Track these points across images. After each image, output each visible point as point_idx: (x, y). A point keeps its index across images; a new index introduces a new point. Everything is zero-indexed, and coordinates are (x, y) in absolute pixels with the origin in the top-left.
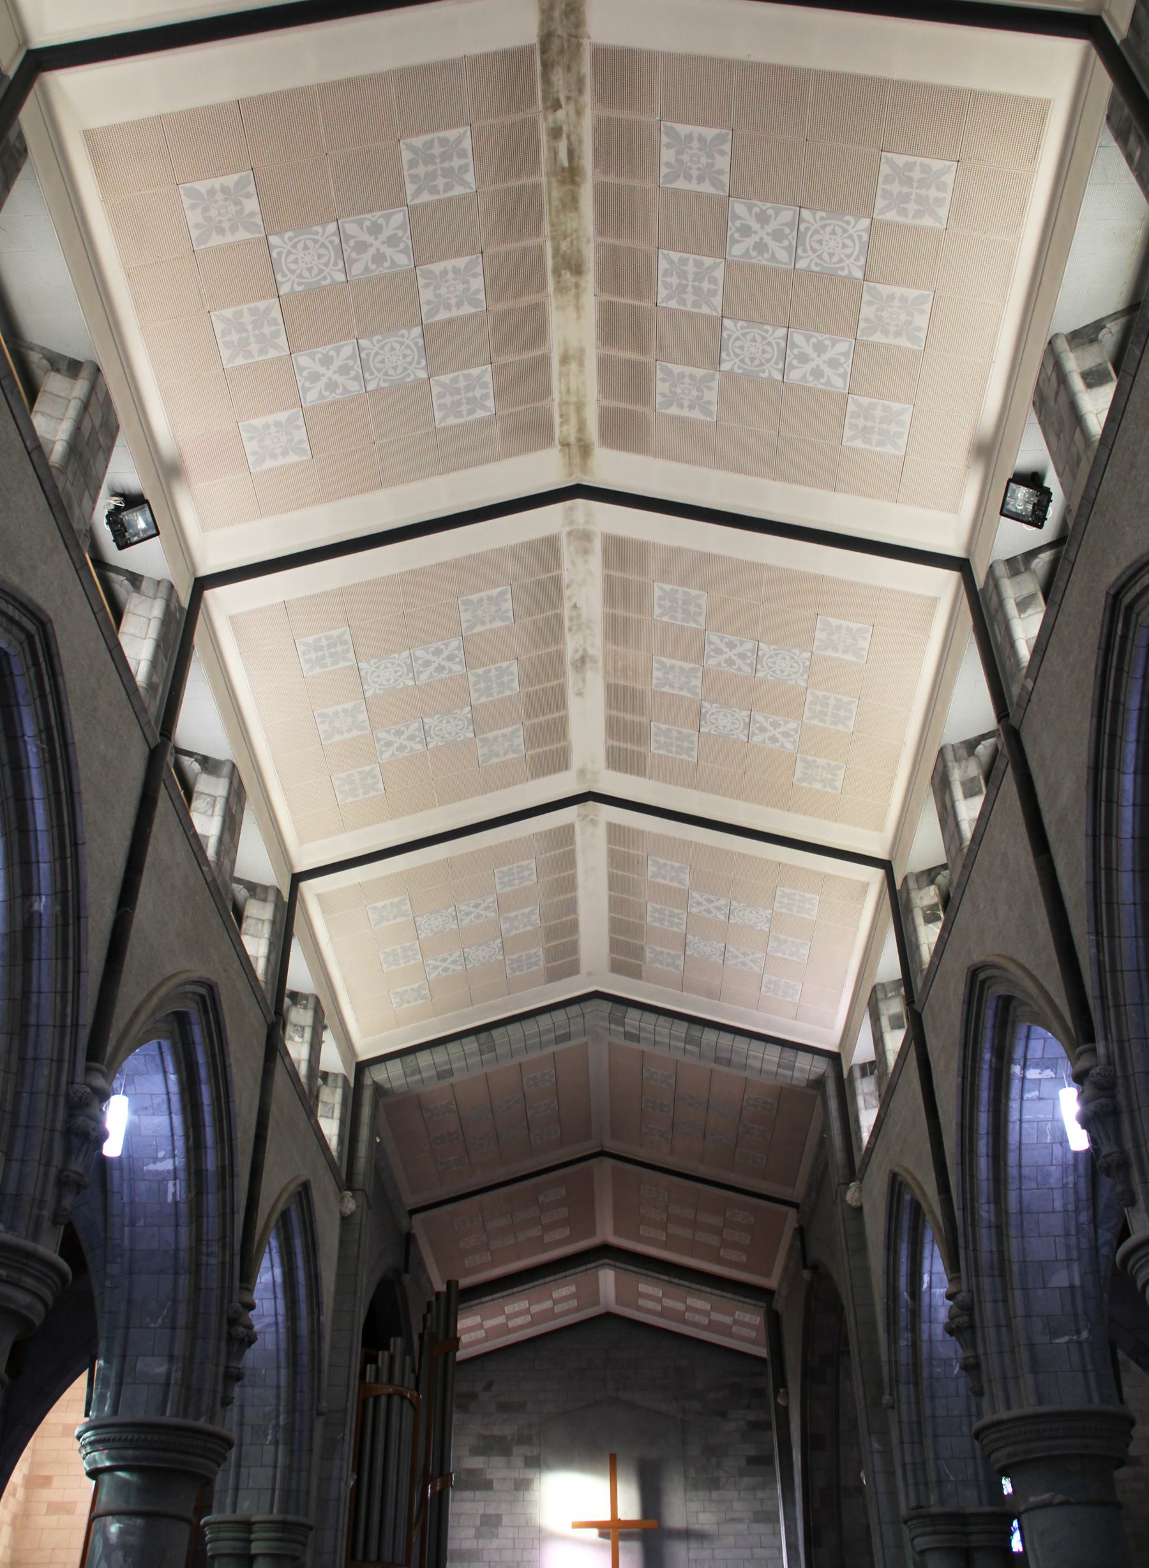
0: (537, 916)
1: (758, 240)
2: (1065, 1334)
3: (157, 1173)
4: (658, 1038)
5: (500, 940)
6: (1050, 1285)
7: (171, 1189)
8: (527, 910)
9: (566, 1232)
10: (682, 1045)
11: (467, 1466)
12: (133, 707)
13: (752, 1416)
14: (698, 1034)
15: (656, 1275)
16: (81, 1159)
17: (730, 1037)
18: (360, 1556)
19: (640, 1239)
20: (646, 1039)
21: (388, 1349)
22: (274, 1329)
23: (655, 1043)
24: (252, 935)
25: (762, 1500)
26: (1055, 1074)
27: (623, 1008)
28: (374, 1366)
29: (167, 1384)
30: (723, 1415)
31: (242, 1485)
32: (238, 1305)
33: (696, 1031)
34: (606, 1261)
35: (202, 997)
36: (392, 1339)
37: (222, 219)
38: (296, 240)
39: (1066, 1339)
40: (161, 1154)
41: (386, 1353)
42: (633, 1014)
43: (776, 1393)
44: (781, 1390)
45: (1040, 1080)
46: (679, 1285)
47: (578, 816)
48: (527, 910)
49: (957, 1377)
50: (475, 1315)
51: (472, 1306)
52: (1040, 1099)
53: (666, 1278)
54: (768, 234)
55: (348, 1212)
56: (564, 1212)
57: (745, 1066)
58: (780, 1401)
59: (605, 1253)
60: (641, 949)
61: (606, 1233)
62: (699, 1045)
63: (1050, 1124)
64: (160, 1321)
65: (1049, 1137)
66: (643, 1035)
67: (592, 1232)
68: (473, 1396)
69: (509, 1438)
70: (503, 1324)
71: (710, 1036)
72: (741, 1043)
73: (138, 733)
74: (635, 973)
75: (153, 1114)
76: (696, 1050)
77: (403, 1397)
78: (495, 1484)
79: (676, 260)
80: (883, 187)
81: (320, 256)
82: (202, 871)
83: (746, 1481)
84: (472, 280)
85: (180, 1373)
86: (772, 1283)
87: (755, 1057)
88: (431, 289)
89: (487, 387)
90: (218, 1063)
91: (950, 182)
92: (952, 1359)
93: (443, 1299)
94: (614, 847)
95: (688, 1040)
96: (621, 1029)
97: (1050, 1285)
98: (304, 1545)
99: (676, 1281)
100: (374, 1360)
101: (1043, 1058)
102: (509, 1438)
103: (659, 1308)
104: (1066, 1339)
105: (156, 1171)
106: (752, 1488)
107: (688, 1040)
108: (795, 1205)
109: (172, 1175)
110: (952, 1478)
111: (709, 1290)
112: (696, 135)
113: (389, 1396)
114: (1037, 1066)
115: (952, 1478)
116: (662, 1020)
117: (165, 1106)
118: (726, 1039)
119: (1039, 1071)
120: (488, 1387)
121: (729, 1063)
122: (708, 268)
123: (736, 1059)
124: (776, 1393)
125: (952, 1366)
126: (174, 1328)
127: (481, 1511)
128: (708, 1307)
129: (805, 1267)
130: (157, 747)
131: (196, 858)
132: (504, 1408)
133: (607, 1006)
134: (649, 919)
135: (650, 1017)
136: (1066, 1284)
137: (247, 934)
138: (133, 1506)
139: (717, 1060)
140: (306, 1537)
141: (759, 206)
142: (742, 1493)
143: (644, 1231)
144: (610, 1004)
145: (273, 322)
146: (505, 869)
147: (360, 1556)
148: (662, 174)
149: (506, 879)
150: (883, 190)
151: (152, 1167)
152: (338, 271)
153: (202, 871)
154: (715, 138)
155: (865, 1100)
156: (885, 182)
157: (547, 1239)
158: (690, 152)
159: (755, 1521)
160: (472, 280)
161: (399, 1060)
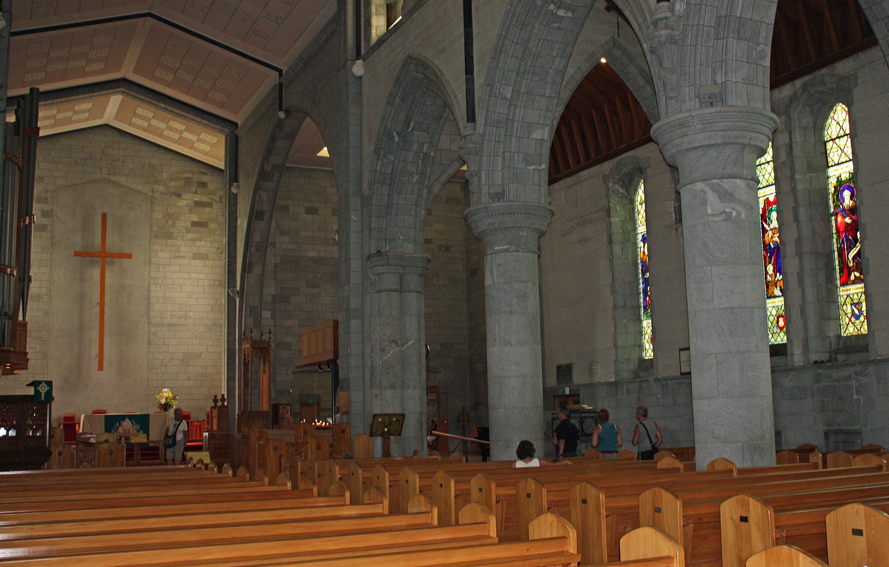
2: (533, 165)
6: (531, 137)
13: (197, 198)
15: (157, 103)
19: (152, 78)
25: (199, 247)
26: (573, 15)
30: (179, 196)
39: (534, 167)
44: (235, 184)
45: (563, 17)
46: (172, 111)
49: (414, 183)
50: (184, 124)
52: (559, 28)
53: (163, 106)
58: (234, 190)
59: (123, 84)
61: (127, 72)
63: (558, 45)
65: (555, 52)
70: (187, 131)
86: (238, 119)
92: (414, 173)
97: (531, 137)
99: (171, 109)
101: (571, 4)
103: (146, 125)
104: (534, 167)
108: (280, 71)
110: (401, 238)
111: (192, 117)
114: (565, 9)
115: (401, 238)
119: (565, 11)
125: (413, 177)
128: (183, 128)
136: (540, 138)
142: (187, 242)
143: (158, 73)
155: (376, 9)
159: (194, 259)
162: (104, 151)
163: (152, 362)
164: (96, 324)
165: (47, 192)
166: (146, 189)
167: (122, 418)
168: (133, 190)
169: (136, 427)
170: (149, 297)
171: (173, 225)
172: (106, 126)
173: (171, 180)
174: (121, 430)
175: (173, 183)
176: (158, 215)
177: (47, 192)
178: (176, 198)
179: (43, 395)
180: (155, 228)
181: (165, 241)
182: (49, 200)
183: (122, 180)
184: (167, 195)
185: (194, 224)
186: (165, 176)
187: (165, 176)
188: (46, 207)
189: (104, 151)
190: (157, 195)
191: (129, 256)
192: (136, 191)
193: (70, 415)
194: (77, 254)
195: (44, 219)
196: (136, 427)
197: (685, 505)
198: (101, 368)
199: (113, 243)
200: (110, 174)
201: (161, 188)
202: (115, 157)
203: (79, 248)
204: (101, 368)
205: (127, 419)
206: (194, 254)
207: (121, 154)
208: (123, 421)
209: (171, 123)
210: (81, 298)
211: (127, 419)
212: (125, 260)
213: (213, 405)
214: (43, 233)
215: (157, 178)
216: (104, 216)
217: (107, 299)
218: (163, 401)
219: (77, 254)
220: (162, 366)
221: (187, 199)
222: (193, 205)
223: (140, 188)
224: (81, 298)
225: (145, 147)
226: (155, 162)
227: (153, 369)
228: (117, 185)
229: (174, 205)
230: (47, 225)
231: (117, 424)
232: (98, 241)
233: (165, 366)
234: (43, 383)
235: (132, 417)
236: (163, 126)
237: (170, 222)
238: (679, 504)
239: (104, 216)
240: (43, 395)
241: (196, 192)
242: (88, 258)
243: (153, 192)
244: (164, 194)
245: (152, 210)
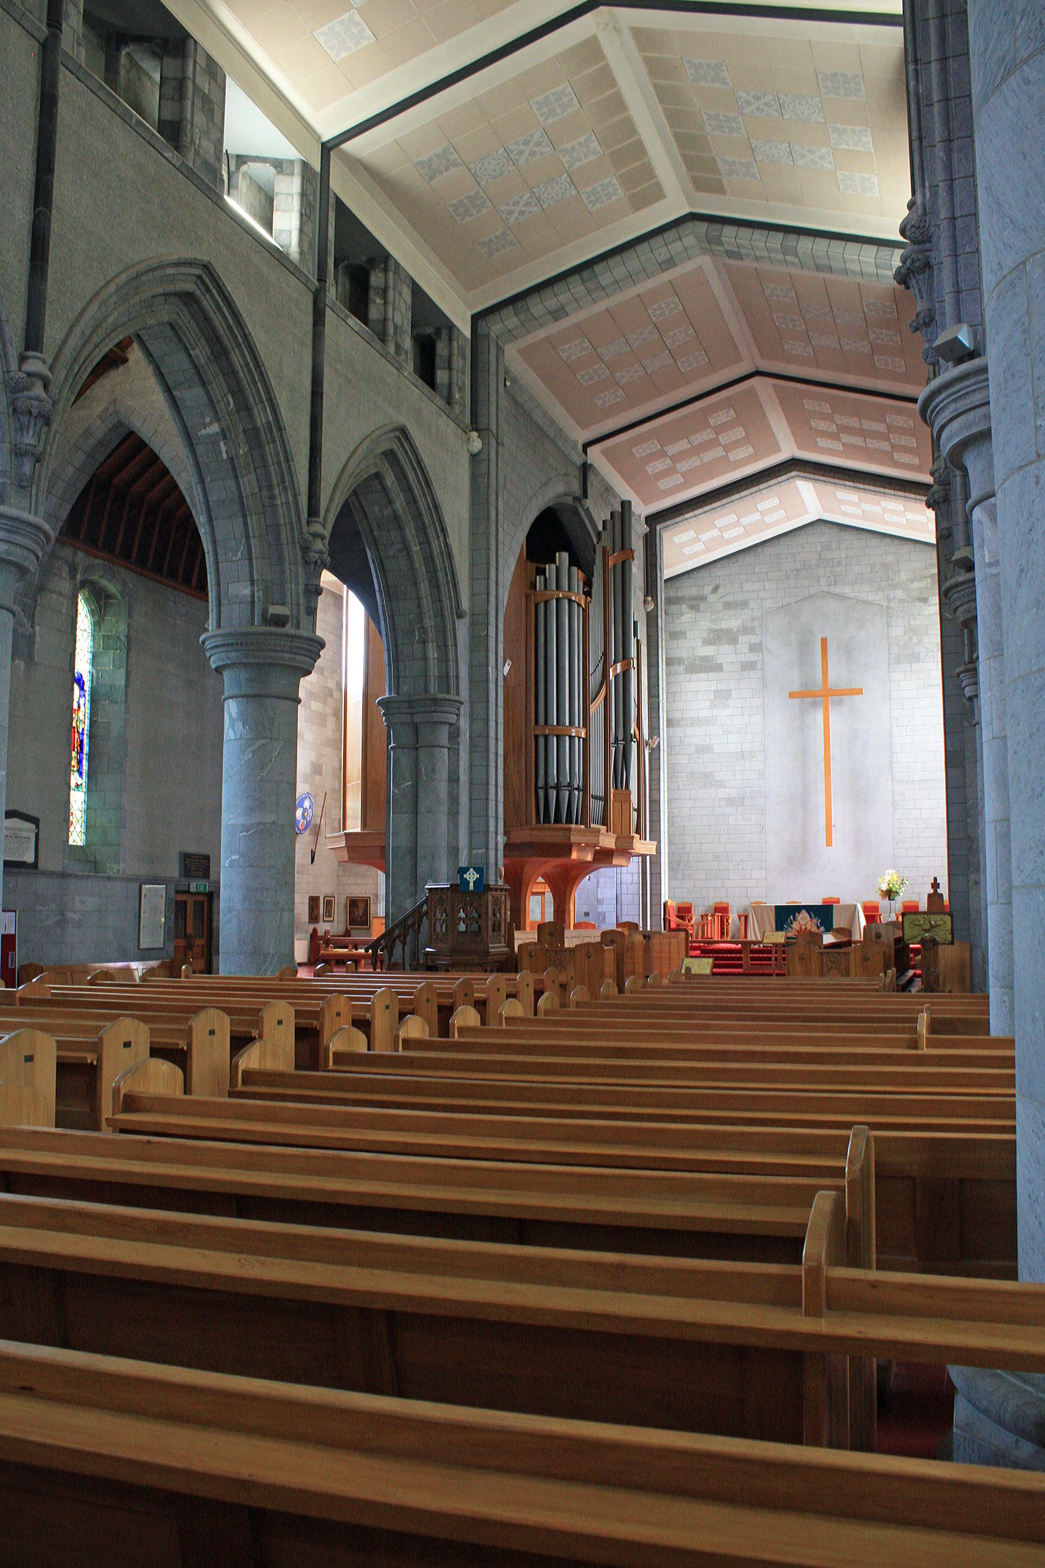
0: (596, 144)
3: (209, 436)
4: (758, 253)
5: (566, 175)
7: (224, 449)
8: (582, 139)
9: (748, 450)
10: (781, 257)
11: (701, 654)
14: (792, 243)
16: (31, 432)
17: (825, 242)
18: (542, 721)
20: (747, 255)
21: (555, 562)
22: (404, 553)
23: (757, 259)
24: (284, 211)
27: (718, 227)
28: (542, 577)
29: (253, 602)
31: (402, 674)
32: (308, 535)
33: (791, 240)
34: (794, 473)
35: (199, 277)
36: (557, 554)
40: (208, 420)
41: (553, 566)
42: (729, 231)
47: (598, 25)
48: (582, 139)
51: (668, 526)
53: (851, 484)
55: (476, 450)
56: (739, 433)
57: (846, 272)
60: (713, 161)
61: (788, 450)
62: (797, 255)
64: (239, 554)
66: (743, 251)
67: (777, 449)
68: (702, 598)
69: (735, 630)
71: (805, 244)
72: (837, 246)
73: (15, 29)
74: (718, 188)
75: (190, 388)
76: (796, 260)
77: (570, 601)
78: (725, 667)
82: (165, 157)
85: (261, 593)
87: (851, 261)
90: (237, 333)
93: (617, 517)
94: (648, 54)
95: (785, 250)
96: (721, 248)
98: (458, 715)
100: (541, 572)
102: (735, 630)
105: (208, 434)
107: (785, 250)
109: (221, 437)
113: (558, 600)
116: (758, 234)
117: (196, 379)
118: (822, 244)
120: (715, 590)
121: (830, 270)
123: (835, 265)
126: (250, 559)
127: (714, 688)
130: (46, 40)
131: (152, 146)
132: (729, 606)
133: (702, 227)
134: (709, 128)
135: (746, 232)
137: (278, 210)
138: (243, 692)
139: (818, 268)
140: (459, 710)
144: (706, 224)
146: (540, 98)
147: (542, 721)
149: (546, 109)
151: (203, 432)
153: (165, 157)
154: (574, 163)
157: (732, 457)
161: (511, 307)
162: (820, 556)
163: (900, 833)
164: (821, 785)
165: (753, 619)
166: (879, 598)
167: (797, 909)
168: (863, 601)
169: (815, 921)
170: (891, 745)
171: (920, 642)
172: (820, 522)
173: (913, 580)
174: (795, 925)
175: (915, 585)
176: (897, 632)
177: (753, 619)
178: (920, 604)
179: (471, 885)
180: (895, 649)
181: (909, 665)
182: (757, 629)
183: (847, 590)
184: (908, 602)
186: (903, 577)
187: (903, 577)
188: (753, 639)
189: (820, 556)
190: (893, 604)
191: (859, 692)
192: (867, 602)
193: (722, 905)
194: (792, 695)
195: (752, 654)
196: (815, 921)
197: (232, 1022)
198: (829, 843)
199: (836, 674)
200: (830, 585)
201: (900, 594)
202: (835, 561)
203: (796, 688)
204: (829, 843)
205: (804, 911)
207: (843, 556)
208: (799, 913)
209: (760, 507)
210: (803, 752)
211: (804, 911)
212: (856, 697)
213: (932, 891)
214: (751, 672)
215: (892, 580)
216: (824, 641)
217: (833, 751)
218: (885, 887)
219: (792, 695)
220: (912, 837)
223: (871, 597)
224: (803, 752)
225: (874, 542)
226: (890, 559)
227: (900, 842)
228: (841, 597)
229: (918, 615)
230: (756, 662)
231: (792, 917)
232: (819, 675)
233: (917, 837)
234: (471, 870)
235: (809, 909)
236: (756, 516)
237: (915, 639)
238: (997, 1029)
239: (824, 641)
240: (471, 885)
242: (809, 700)
243: (889, 601)
244: (904, 601)
245: (888, 626)
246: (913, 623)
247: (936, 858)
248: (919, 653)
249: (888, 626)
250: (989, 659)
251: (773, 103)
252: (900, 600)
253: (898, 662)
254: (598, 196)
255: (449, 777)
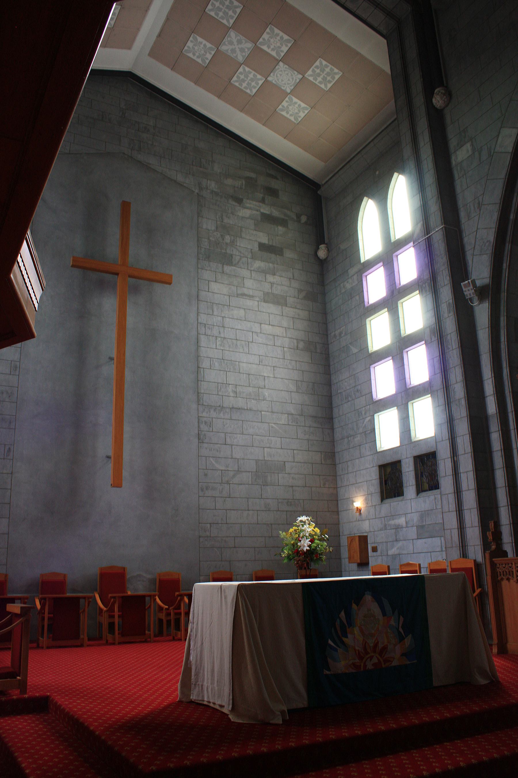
1: (234, 48)
12: (240, 330)
13: (266, 210)
25: (272, 284)
30: (239, 201)
37: (273, 44)
38: (294, 81)
43: (429, 95)
54: (234, 45)
58: (438, 101)
79: (249, 90)
80: (234, 15)
81: (289, 80)
83: (258, 264)
84: (285, 106)
88: (281, 49)
89: (235, 14)
91: (238, 12)
106: (264, 272)
112: (270, 49)
122: (238, 82)
124: (429, 95)
129: (297, 561)
141: (240, 37)
145: (235, 13)
148: (308, 111)
150: (235, 15)
152: (290, 89)
154: (264, 45)
156: (233, 17)
158: (275, 45)
160: (285, 106)
163: (206, 475)
171: (233, 242)
175: (229, 182)
181: (220, 265)
185: (262, 247)
187: (217, 168)
198: (117, 483)
206: (266, 294)
216: (126, 207)
221: (250, 208)
222: (259, 218)
223: (180, 178)
227: (207, 488)
233: (228, 483)
237: (228, 239)
239: (126, 207)
241: (263, 201)
243: (201, 189)
246: (226, 220)
247: (251, 513)
248: (232, 256)
249: (199, 214)
250: (399, 368)
251: (246, 50)
252: (212, 192)
253: (208, 258)
254: (227, 10)
255: (341, 560)
